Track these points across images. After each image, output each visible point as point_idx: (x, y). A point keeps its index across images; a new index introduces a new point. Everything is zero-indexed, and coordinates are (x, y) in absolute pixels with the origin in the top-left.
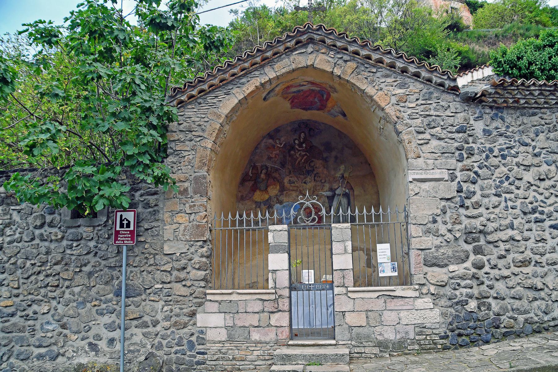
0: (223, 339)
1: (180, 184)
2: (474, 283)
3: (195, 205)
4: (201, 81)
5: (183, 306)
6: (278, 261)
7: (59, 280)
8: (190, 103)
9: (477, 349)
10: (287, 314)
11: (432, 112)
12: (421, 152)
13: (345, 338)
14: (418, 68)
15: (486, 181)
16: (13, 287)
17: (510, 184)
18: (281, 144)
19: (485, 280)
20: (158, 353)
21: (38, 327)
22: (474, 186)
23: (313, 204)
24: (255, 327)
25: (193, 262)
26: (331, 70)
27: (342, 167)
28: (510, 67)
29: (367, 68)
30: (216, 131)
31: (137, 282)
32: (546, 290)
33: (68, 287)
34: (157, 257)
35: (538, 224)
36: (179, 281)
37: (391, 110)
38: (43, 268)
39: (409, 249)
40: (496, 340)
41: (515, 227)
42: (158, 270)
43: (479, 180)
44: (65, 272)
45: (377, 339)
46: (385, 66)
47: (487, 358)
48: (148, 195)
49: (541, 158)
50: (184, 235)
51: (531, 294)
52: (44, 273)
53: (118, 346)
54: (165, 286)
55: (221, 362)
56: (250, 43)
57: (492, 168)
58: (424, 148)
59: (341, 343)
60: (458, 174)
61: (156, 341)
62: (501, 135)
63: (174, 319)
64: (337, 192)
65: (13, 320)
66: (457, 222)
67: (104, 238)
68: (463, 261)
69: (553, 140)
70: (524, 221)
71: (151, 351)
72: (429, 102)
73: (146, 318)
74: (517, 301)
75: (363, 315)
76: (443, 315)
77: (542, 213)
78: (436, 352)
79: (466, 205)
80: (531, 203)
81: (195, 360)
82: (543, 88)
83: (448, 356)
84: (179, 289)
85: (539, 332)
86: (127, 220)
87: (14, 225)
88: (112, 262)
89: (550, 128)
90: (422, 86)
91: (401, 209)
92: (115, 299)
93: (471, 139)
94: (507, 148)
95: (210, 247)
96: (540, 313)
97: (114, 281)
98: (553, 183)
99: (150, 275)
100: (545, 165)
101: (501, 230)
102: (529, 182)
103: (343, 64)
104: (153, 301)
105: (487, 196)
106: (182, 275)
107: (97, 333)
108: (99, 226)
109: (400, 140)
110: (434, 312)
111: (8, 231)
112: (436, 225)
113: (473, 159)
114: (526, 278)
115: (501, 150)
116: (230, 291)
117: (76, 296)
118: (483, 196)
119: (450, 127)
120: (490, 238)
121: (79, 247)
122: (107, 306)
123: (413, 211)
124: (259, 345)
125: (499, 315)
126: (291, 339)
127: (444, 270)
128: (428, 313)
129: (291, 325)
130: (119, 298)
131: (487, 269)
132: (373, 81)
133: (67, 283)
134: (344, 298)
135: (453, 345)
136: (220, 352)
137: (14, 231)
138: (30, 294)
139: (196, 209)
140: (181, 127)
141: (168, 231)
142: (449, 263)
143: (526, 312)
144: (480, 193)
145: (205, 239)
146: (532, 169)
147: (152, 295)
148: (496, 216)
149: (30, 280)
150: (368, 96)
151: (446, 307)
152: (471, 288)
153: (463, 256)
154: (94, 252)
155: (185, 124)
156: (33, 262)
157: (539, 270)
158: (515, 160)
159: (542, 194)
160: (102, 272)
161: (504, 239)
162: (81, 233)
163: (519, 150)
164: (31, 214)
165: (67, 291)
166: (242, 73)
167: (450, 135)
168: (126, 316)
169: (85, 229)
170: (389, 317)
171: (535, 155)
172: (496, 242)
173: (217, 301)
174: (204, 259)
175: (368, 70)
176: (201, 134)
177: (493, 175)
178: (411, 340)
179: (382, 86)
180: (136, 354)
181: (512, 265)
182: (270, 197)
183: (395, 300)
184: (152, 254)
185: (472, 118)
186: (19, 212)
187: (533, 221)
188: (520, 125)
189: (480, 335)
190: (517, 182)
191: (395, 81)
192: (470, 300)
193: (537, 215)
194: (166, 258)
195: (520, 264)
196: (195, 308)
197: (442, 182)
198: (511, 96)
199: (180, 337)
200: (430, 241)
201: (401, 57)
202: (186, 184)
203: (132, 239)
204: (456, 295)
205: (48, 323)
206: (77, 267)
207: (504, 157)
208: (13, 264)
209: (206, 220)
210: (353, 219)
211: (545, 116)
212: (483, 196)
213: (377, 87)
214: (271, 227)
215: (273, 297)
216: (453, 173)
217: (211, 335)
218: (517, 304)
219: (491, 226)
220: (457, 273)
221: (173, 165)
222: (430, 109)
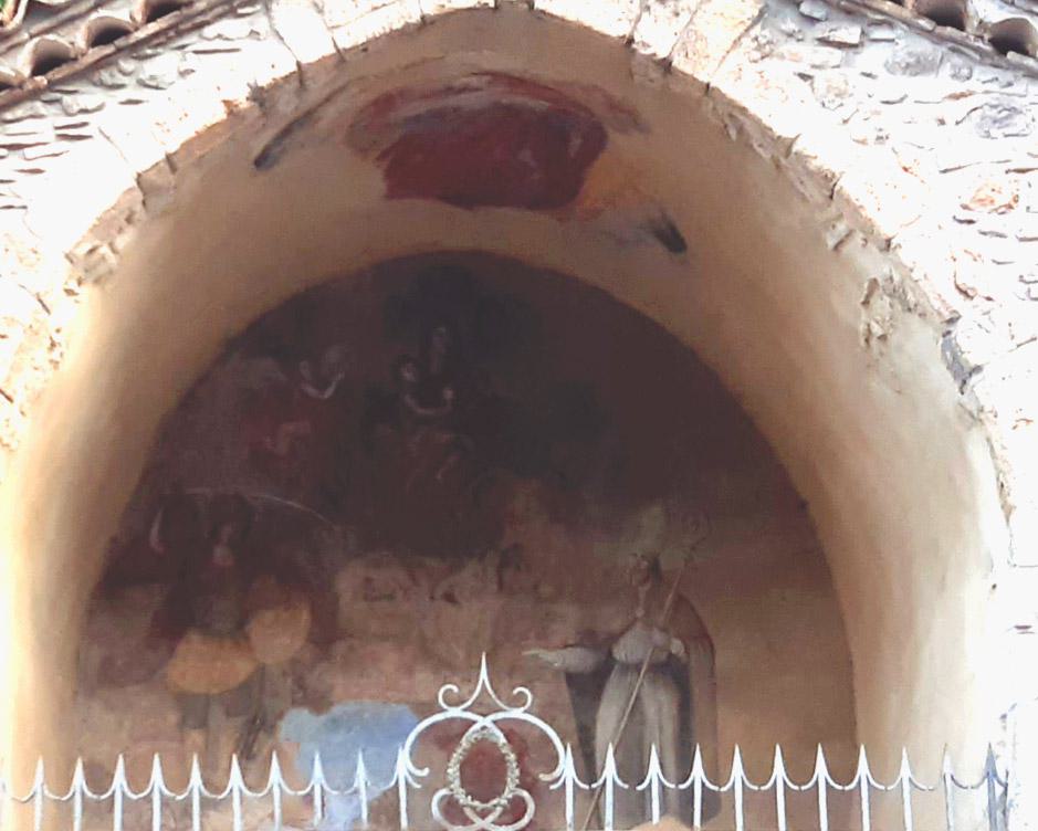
18: (322, 384)
23: (511, 730)
27: (652, 519)
29: (812, 20)
64: (621, 653)
91: (972, 770)
109: (972, 407)
150: (810, 174)
166: (153, 27)
175: (820, 30)
182: (261, 671)
213: (859, 128)
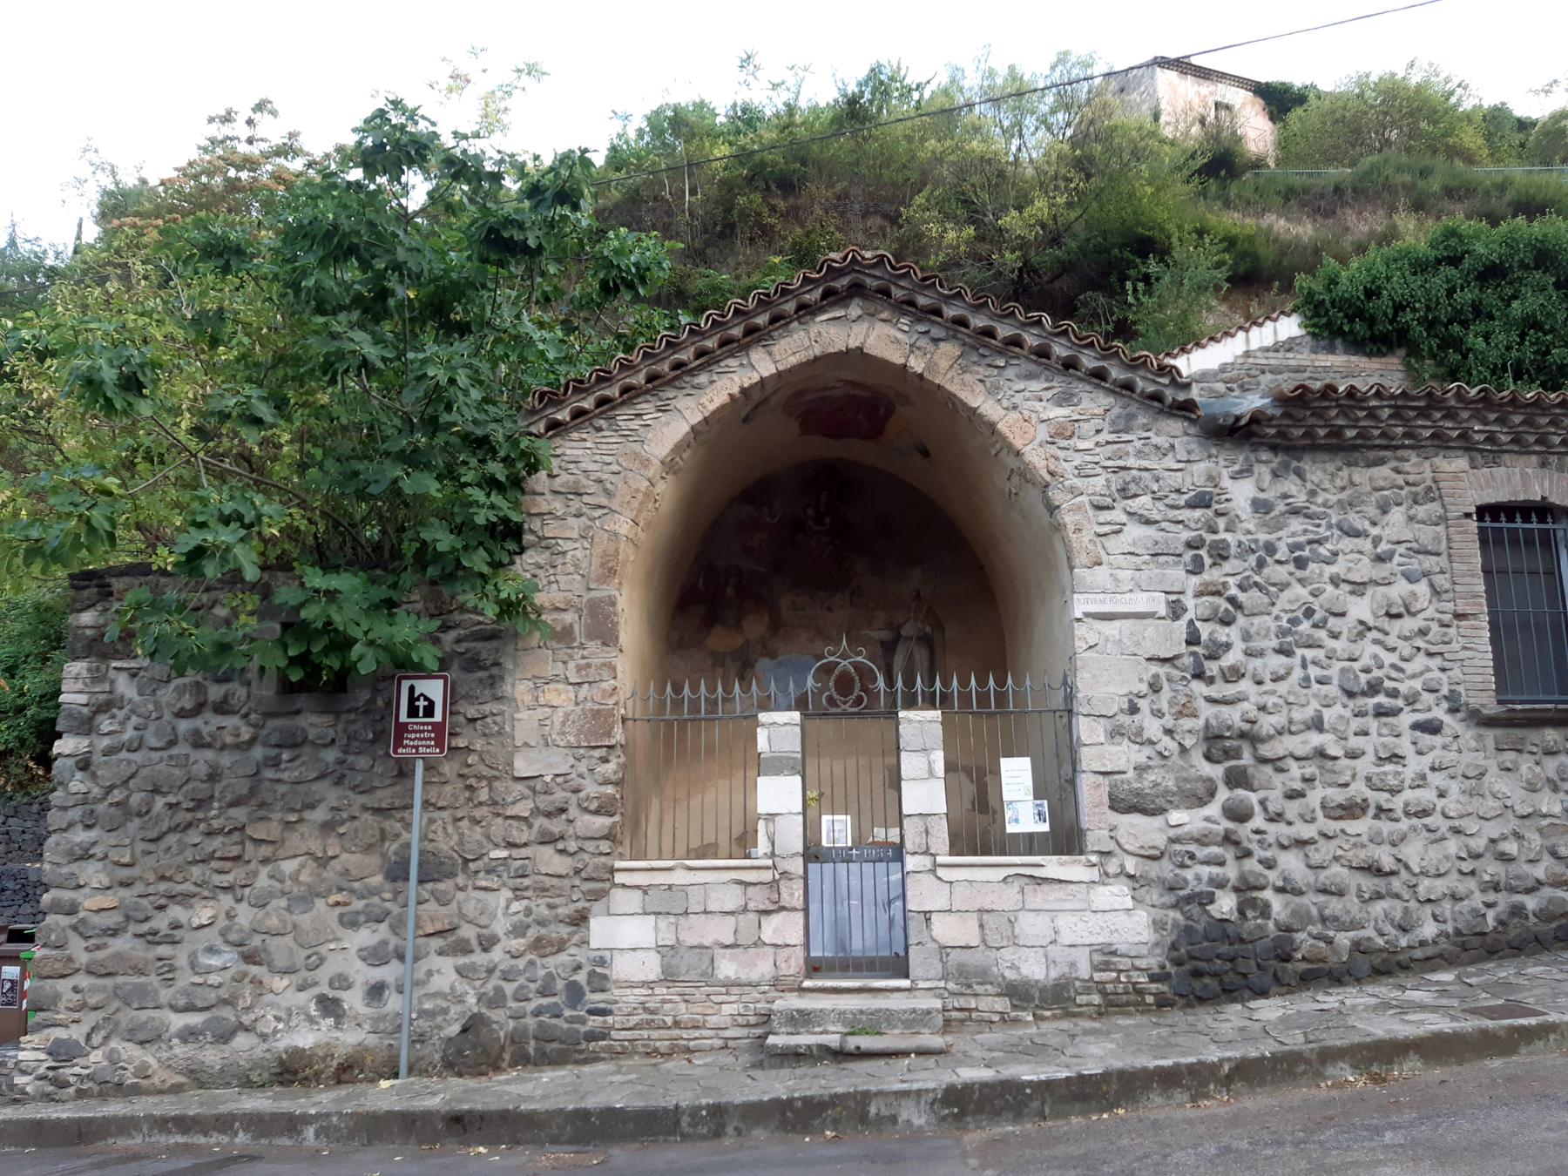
0: (652, 977)
1: (555, 615)
2: (1229, 854)
3: (589, 666)
4: (604, 379)
5: (557, 901)
6: (779, 795)
7: (242, 843)
8: (577, 428)
9: (1239, 1007)
10: (799, 917)
11: (1131, 462)
12: (1103, 553)
13: (932, 973)
14: (1104, 358)
15: (1256, 620)
16: (117, 864)
17: (1315, 626)
19: (1254, 847)
20: (497, 1015)
21: (182, 961)
22: (1227, 630)
23: (856, 666)
24: (727, 947)
25: (582, 795)
26: (902, 361)
28: (1346, 316)
30: (640, 496)
31: (445, 845)
32: (1404, 874)
33: (265, 861)
34: (496, 784)
35: (1384, 720)
36: (548, 839)
37: (1036, 457)
38: (200, 815)
39: (1074, 770)
40: (1284, 990)
41: (1326, 726)
42: (499, 815)
43: (1239, 616)
44: (259, 825)
45: (1004, 977)
46: (1025, 353)
47: (1258, 1026)
48: (475, 640)
49: (1393, 565)
50: (564, 733)
51: (1368, 883)
52: (202, 826)
53: (393, 1002)
54: (516, 853)
55: (645, 1034)
56: (665, 207)
57: (1273, 589)
58: (1111, 543)
59: (921, 984)
60: (1189, 601)
61: (490, 986)
62: (1295, 512)
63: (532, 933)
64: (903, 632)
65: (118, 944)
66: (1186, 711)
67: (365, 741)
68: (1202, 802)
69: (1424, 523)
70: (1348, 713)
71: (475, 1010)
72: (1125, 437)
73: (468, 932)
74: (1334, 899)
75: (972, 922)
76: (1158, 925)
77: (1394, 694)
78: (1142, 1013)
79: (1208, 673)
80: (1367, 671)
81: (583, 1029)
82: (1400, 403)
83: (1170, 1021)
84: (549, 860)
85: (1388, 973)
86: (426, 699)
87: (121, 708)
88: (383, 797)
89: (1416, 494)
90: (1111, 400)
91: (1057, 683)
92: (388, 886)
93: (1221, 523)
94: (1310, 542)
95: (622, 760)
96: (1388, 928)
97: (387, 844)
98: (1423, 624)
99: (478, 829)
100: (1404, 582)
101: (1291, 733)
102: (1361, 623)
103: (930, 347)
104: (485, 889)
105: (1261, 654)
106: (556, 826)
107: (340, 970)
108: (349, 711)
110: (1136, 918)
111: (105, 724)
112: (1136, 717)
113: (1227, 567)
114: (1355, 845)
115: (1294, 547)
116: (671, 863)
117: (289, 883)
118: (1249, 653)
119: (1173, 496)
120: (1266, 750)
121: (298, 762)
122: (367, 906)
123: (1085, 685)
124: (735, 990)
125: (1289, 929)
126: (808, 977)
127: (1157, 821)
128: (1121, 920)
129: (807, 945)
130: (399, 885)
131: (1258, 821)
132: (998, 388)
133: (265, 851)
134: (928, 879)
135: (1181, 996)
136: (645, 1009)
137: (122, 723)
138: (163, 878)
139: (593, 674)
140: (557, 484)
141: (525, 723)
142: (1165, 805)
143: (1354, 925)
144: (1243, 646)
145: (613, 742)
146: (1370, 591)
147: (481, 875)
148: (1281, 701)
149: (163, 845)
151: (1164, 906)
152: (1222, 864)
153: (1201, 790)
154: (337, 774)
155: (564, 477)
156: (171, 799)
157: (1386, 826)
158: (1330, 570)
159: (1393, 650)
160: (356, 823)
161: (1299, 753)
162: (303, 730)
163: (1340, 546)
164: (168, 682)
165: (264, 871)
167: (1172, 514)
168: (418, 926)
169: (314, 719)
170: (1032, 927)
171: (1380, 559)
172: (1280, 759)
173: (638, 887)
174: (610, 790)
175: (988, 361)
176: (604, 501)
177: (1273, 604)
178: (1083, 981)
179: (1018, 399)
180: (439, 1019)
181: (1319, 814)
183: (1046, 887)
184: (484, 777)
185: (1225, 473)
186: (134, 676)
187: (1371, 712)
188: (1343, 489)
189: (1245, 976)
190: (1332, 621)
191: (1047, 389)
192: (1219, 893)
193: (1381, 699)
194: (520, 788)
195: (1340, 812)
196: (587, 905)
197: (1150, 621)
198: (1321, 423)
199: (550, 975)
200: (1124, 756)
201: (1065, 333)
202: (569, 617)
203: (439, 744)
204: (1185, 881)
205: (211, 950)
206: (292, 810)
207: (1301, 563)
208: (117, 804)
209: (615, 699)
210: (946, 700)
211: (1407, 466)
212: (1249, 653)
213: (1005, 403)
214: (763, 717)
215: (767, 876)
216: (1178, 601)
217: (623, 968)
218: (1334, 906)
219: (1267, 723)
220: (1186, 829)
221: (539, 572)
222: (1127, 454)
